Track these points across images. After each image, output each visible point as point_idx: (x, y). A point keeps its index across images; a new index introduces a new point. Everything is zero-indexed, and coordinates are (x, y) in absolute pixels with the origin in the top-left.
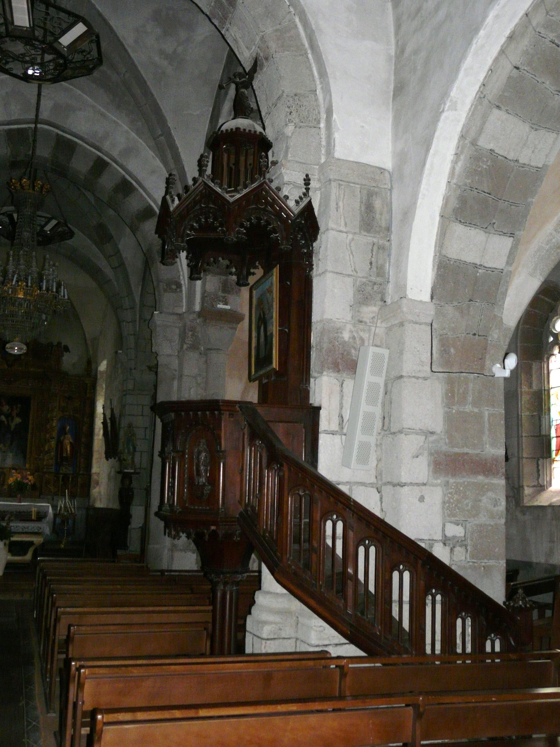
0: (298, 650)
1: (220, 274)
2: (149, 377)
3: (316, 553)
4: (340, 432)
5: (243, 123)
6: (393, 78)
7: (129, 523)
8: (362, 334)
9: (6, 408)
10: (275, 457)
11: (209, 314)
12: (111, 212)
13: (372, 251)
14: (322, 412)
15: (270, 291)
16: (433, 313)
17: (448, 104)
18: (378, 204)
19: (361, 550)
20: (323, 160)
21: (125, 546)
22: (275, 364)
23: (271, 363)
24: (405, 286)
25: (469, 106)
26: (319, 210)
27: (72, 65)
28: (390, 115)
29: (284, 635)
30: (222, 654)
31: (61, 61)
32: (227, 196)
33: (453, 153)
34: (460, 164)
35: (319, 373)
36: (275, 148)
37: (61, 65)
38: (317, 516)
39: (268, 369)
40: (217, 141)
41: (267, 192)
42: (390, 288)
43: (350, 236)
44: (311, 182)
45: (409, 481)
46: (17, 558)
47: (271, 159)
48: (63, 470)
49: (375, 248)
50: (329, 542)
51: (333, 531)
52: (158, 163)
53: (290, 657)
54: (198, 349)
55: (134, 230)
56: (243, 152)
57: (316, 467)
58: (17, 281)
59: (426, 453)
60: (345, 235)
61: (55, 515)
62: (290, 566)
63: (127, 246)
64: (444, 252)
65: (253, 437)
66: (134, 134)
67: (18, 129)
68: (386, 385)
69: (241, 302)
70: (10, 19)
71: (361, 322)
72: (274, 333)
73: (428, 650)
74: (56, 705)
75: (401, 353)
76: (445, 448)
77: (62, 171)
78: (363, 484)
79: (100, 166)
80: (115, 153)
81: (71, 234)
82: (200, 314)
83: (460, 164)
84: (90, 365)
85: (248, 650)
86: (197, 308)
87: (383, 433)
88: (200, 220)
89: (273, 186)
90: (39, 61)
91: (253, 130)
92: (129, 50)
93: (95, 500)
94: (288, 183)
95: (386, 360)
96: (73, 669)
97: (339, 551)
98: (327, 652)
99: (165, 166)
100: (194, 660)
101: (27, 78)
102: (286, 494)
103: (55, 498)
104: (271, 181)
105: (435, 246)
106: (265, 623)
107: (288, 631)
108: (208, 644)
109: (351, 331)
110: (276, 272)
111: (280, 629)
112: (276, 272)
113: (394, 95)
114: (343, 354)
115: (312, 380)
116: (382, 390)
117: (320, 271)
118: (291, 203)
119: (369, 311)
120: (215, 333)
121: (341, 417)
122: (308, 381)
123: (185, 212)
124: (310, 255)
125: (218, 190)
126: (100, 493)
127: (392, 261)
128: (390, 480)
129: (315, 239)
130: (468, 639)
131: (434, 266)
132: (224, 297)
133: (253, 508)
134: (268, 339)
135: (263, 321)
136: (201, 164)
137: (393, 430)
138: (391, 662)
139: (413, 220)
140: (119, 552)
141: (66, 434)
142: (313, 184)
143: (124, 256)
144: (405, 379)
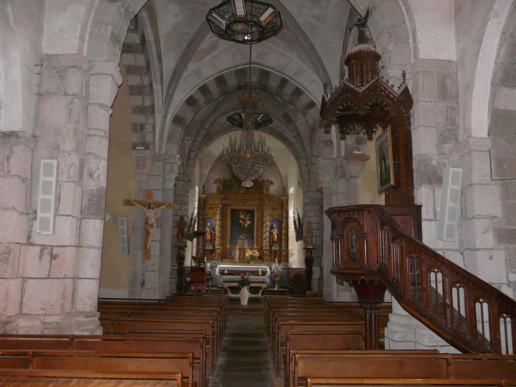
0: (417, 349)
1: (355, 134)
2: (317, 195)
3: (425, 291)
4: (435, 219)
5: (363, 47)
6: (453, 5)
7: (312, 276)
8: (444, 161)
9: (242, 216)
10: (397, 236)
11: (350, 157)
12: (291, 106)
13: (447, 111)
14: (423, 209)
15: (386, 141)
16: (490, 144)
17: (492, 14)
18: (449, 82)
19: (454, 290)
20: (412, 62)
21: (310, 288)
22: (392, 182)
23: (390, 182)
24: (470, 130)
25: (507, 13)
26: (412, 91)
27: (267, 31)
28: (453, 29)
29: (407, 340)
30: (371, 348)
31: (261, 30)
32: (357, 89)
33: (498, 44)
34: (503, 50)
35: (419, 185)
36: (382, 59)
37: (261, 32)
38: (425, 269)
39: (388, 185)
40: (349, 60)
41: (380, 84)
42: (461, 132)
43: (433, 104)
44: (407, 75)
45: (481, 247)
46: (254, 296)
47: (381, 65)
48: (274, 248)
49: (449, 109)
50: (433, 285)
51: (436, 280)
52: (315, 76)
53: (404, 352)
54: (345, 177)
55: (304, 115)
56: (363, 63)
57: (421, 241)
58: (246, 148)
59: (491, 230)
60: (429, 103)
61: (271, 273)
62: (410, 299)
63: (301, 123)
64: (495, 106)
65: (382, 225)
66: (300, 63)
67: (240, 69)
68: (462, 190)
69: (370, 149)
70: (234, 12)
71: (443, 154)
72: (391, 164)
73: (504, 352)
74: (282, 373)
75: (471, 170)
76: (504, 226)
77: (263, 88)
78: (451, 250)
79: (284, 82)
80: (291, 75)
81: (271, 121)
82: (345, 158)
83: (503, 50)
84: (285, 190)
85: (387, 347)
86: (343, 154)
87: (462, 219)
88: (343, 104)
89: (384, 80)
90: (250, 31)
91: (369, 50)
92: (295, 18)
93: (291, 264)
94: (393, 77)
95: (461, 175)
96: (291, 354)
97: (440, 291)
98: (437, 350)
99: (319, 77)
100: (336, 352)
101: (244, 42)
102: (404, 257)
103: (271, 263)
104: (383, 78)
105: (489, 103)
106: (396, 332)
107: (410, 337)
108: (364, 343)
109: (437, 160)
110: (389, 129)
111: (405, 336)
112: (389, 129)
113: (455, 15)
114: (433, 173)
115: (415, 190)
116: (460, 193)
117: (416, 126)
118: (396, 89)
119: (448, 147)
120: (353, 168)
121: (435, 210)
122: (412, 190)
123: (334, 101)
124: (409, 118)
125: (352, 86)
126: (294, 260)
127: (461, 115)
128: (468, 247)
129: (411, 108)
130: (510, 343)
131: (489, 115)
132: (357, 147)
133: (385, 266)
134: (387, 168)
135: (382, 158)
136: (342, 74)
137: (468, 217)
138: (478, 358)
139: (473, 89)
140: (307, 292)
141: (274, 228)
142: (407, 76)
143: (300, 130)
144: (474, 186)
